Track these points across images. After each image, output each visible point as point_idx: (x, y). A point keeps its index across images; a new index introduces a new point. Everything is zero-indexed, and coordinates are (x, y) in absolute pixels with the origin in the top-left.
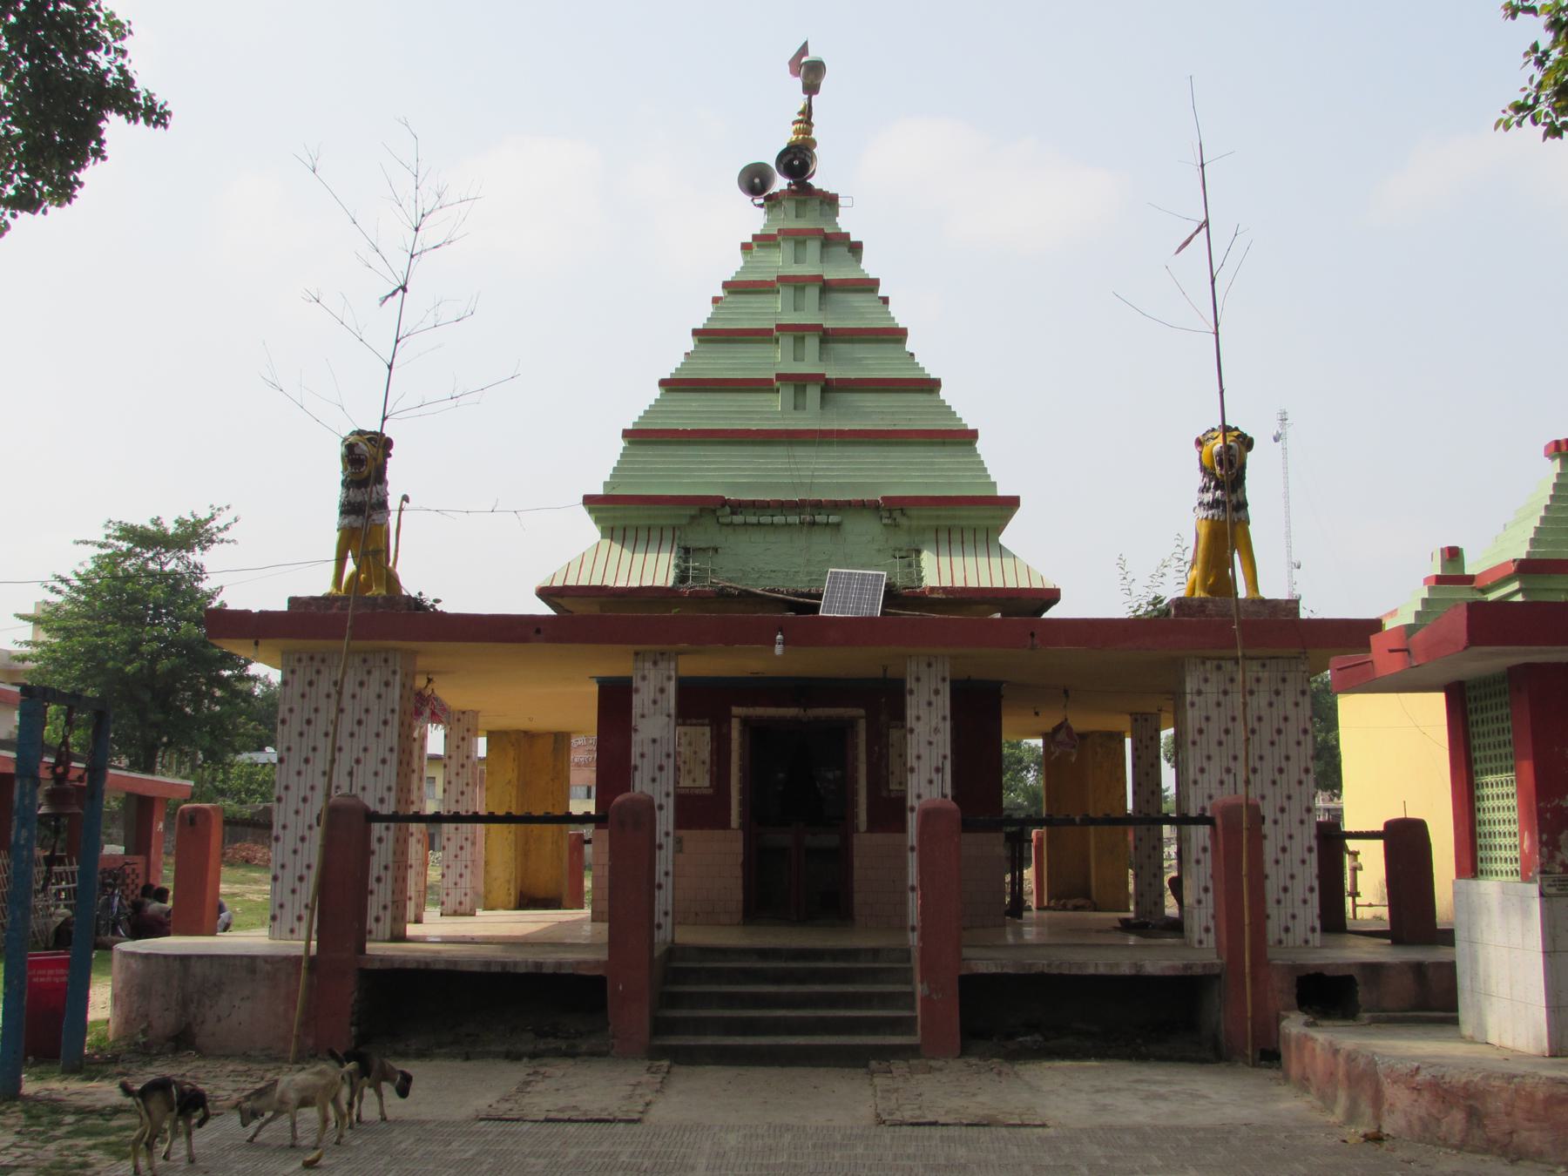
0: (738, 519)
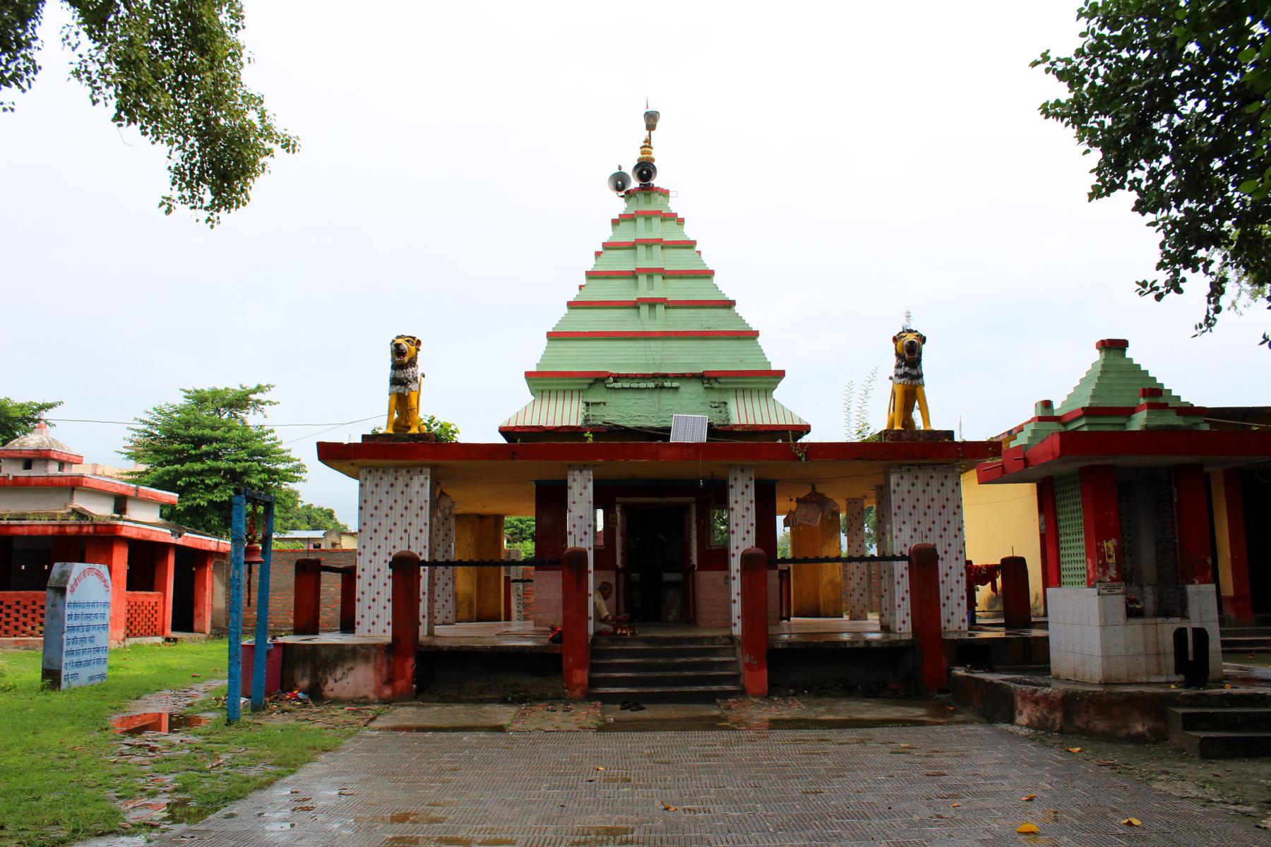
0: (618, 385)
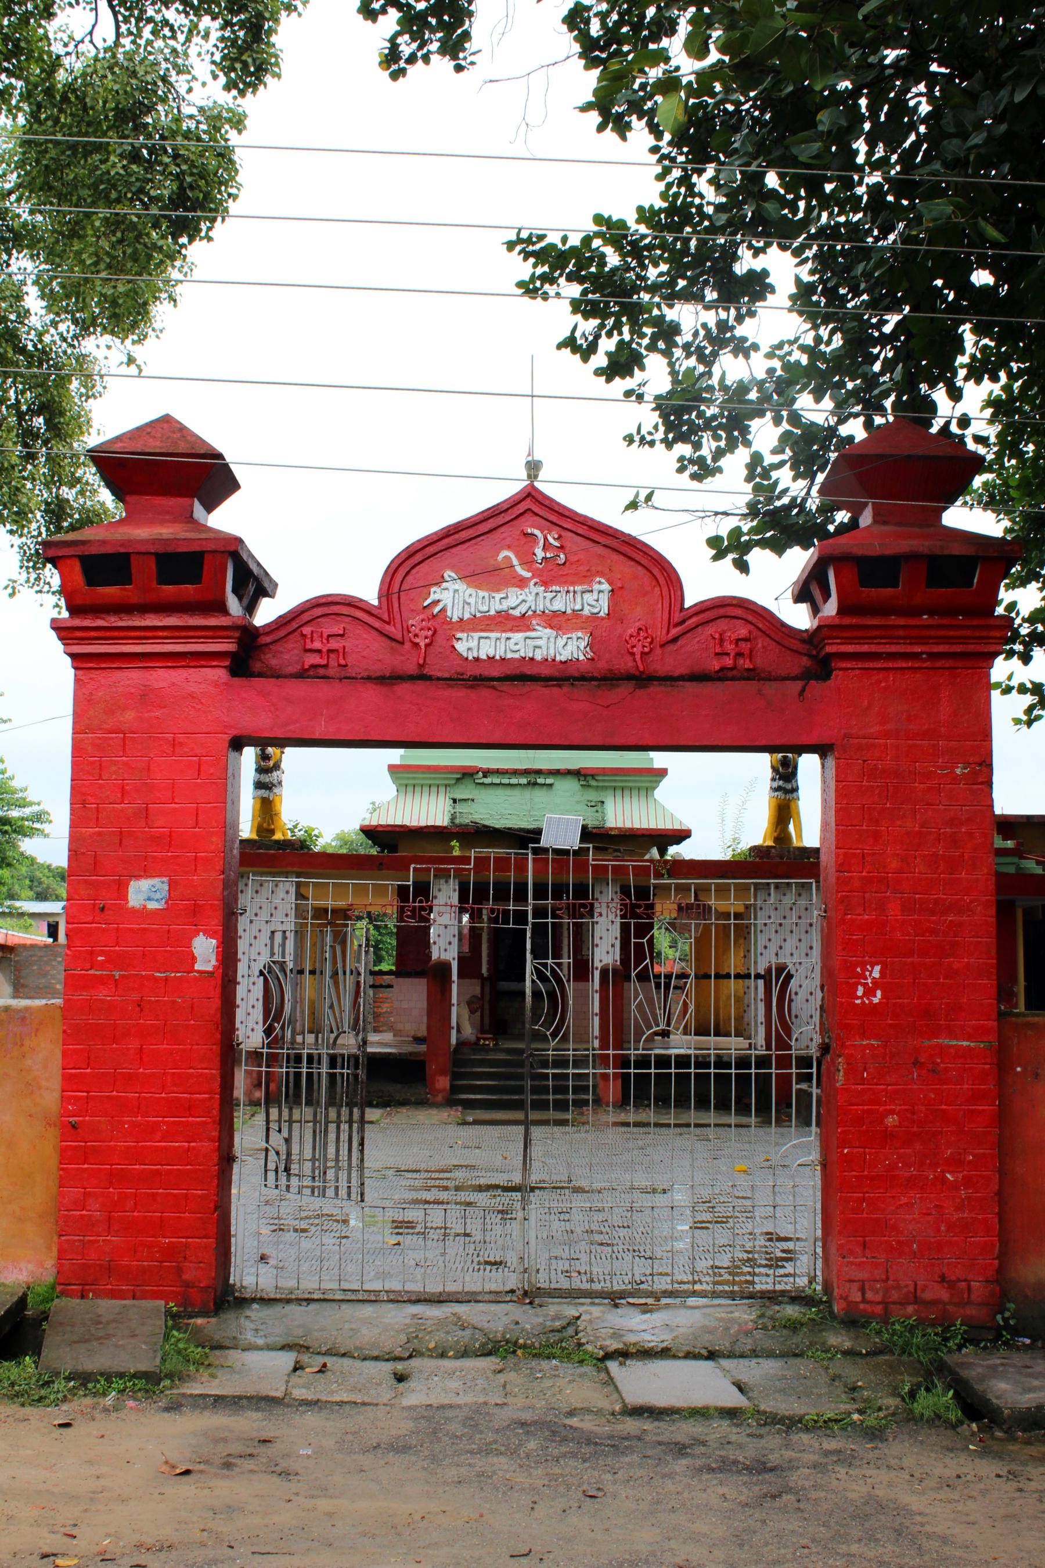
0: (488, 781)
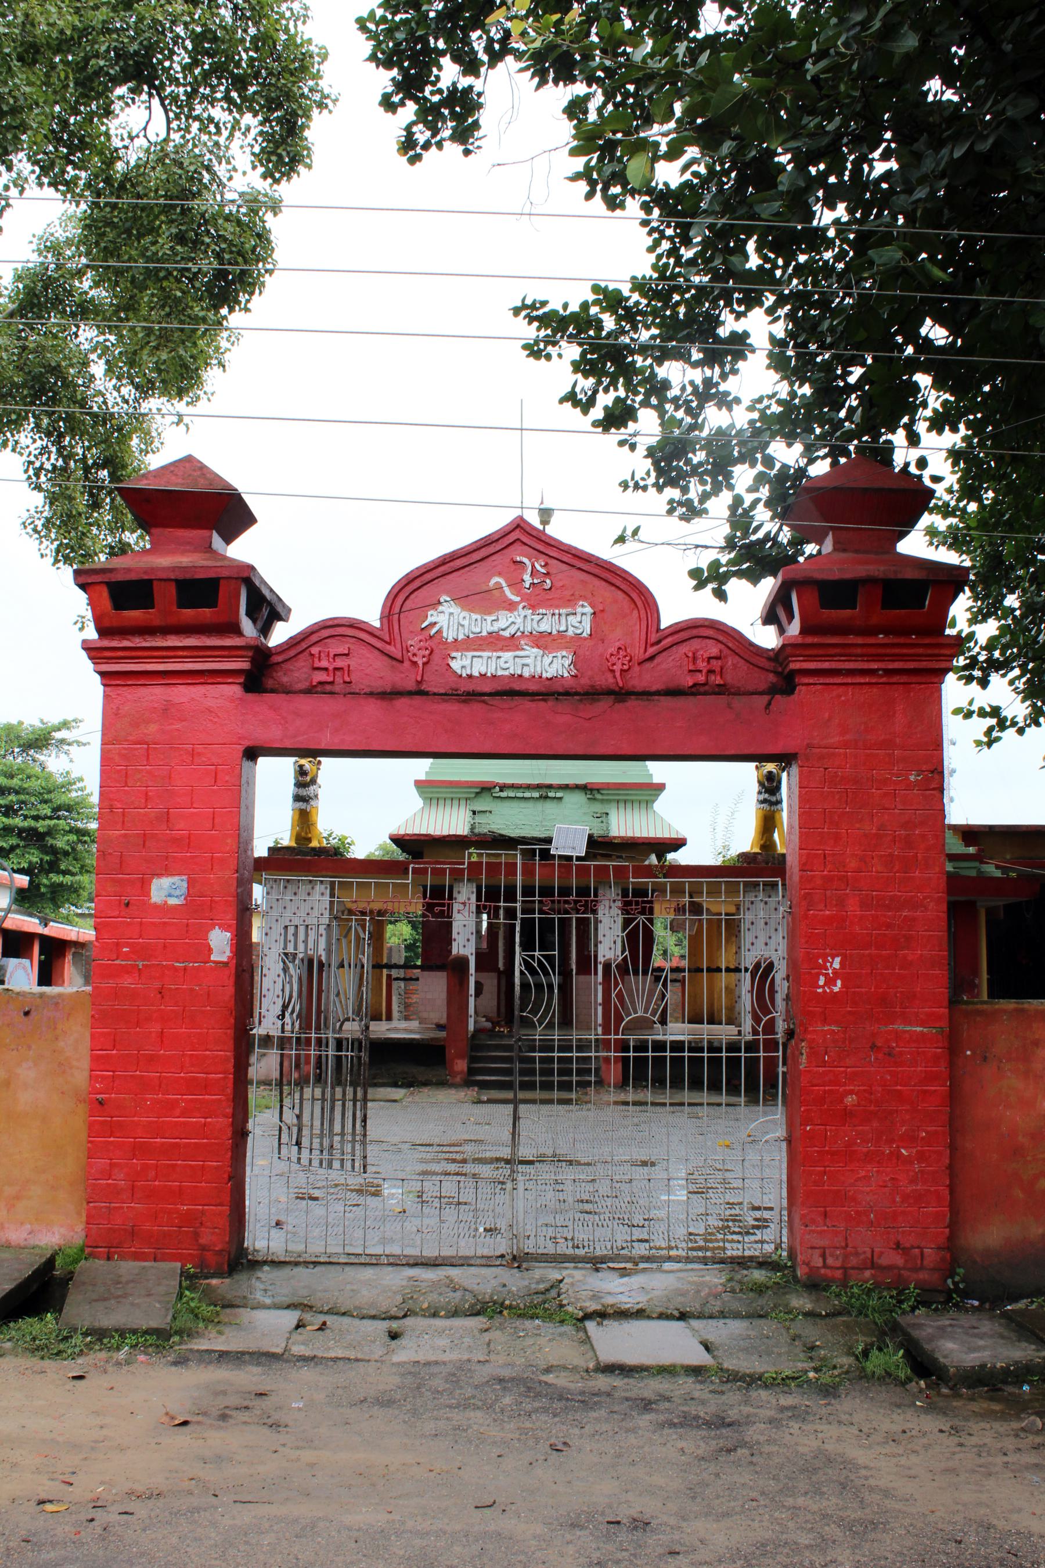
0: (504, 794)
